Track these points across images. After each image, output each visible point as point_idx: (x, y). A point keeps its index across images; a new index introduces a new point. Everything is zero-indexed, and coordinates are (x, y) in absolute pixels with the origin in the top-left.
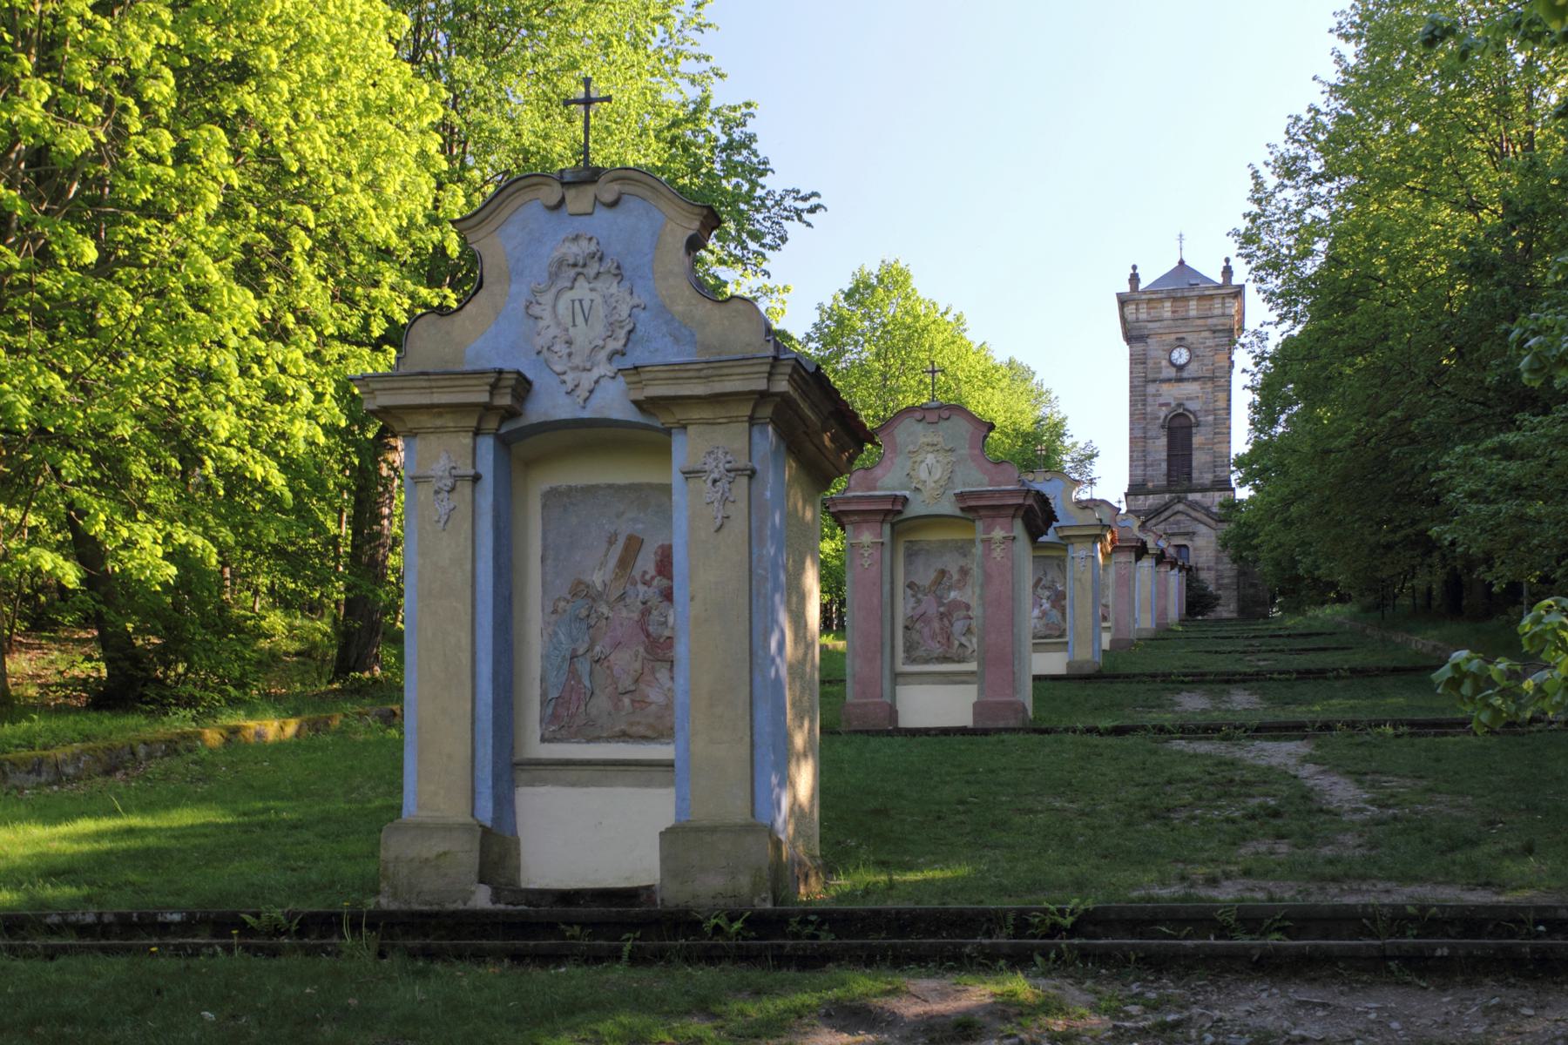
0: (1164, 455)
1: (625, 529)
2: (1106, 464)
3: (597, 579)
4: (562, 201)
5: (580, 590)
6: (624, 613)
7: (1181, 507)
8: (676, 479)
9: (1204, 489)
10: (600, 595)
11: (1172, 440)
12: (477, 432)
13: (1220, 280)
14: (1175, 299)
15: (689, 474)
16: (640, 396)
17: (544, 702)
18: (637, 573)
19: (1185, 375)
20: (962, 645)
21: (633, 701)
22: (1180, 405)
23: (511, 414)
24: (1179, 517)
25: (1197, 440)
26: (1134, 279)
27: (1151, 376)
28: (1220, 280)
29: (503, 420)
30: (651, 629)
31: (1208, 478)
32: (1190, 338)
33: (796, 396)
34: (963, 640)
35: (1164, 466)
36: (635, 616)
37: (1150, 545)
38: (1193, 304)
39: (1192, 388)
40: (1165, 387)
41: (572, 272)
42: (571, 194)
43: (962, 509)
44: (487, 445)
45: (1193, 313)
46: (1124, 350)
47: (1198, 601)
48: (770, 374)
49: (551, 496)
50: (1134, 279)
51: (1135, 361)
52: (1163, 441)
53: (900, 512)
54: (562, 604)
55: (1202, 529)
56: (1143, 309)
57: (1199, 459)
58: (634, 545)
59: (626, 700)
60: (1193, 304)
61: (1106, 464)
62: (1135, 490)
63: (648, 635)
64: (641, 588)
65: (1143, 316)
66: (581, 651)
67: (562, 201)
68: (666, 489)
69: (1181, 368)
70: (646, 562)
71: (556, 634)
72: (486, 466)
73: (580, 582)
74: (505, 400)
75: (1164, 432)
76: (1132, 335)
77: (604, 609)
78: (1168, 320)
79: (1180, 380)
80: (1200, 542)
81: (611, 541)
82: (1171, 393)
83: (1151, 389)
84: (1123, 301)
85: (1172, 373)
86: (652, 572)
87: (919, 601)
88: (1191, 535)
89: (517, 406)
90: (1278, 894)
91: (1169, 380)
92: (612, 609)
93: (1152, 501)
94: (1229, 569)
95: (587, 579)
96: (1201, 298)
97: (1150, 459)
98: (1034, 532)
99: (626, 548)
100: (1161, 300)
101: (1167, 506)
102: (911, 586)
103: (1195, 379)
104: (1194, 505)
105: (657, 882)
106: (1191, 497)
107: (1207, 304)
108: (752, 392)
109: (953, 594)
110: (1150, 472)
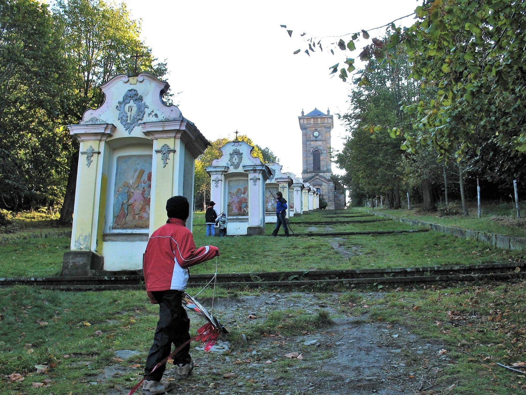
0: (312, 162)
1: (139, 167)
2: (291, 162)
3: (131, 182)
4: (129, 80)
5: (126, 185)
6: (138, 191)
7: (317, 177)
8: (154, 153)
9: (324, 172)
10: (131, 186)
11: (315, 159)
12: (100, 141)
13: (326, 114)
14: (314, 118)
15: (157, 152)
16: (145, 131)
17: (114, 217)
18: (142, 180)
19: (318, 139)
20: (244, 210)
21: (139, 217)
22: (316, 148)
23: (110, 135)
24: (318, 180)
25: (321, 158)
26: (303, 112)
27: (308, 139)
28: (326, 114)
29: (108, 137)
30: (145, 196)
31: (325, 169)
32: (319, 129)
33: (187, 131)
34: (245, 209)
35: (312, 165)
36: (141, 192)
37: (311, 189)
38: (319, 120)
39: (320, 143)
40: (312, 143)
41: (129, 98)
42: (131, 79)
43: (245, 171)
44: (103, 144)
45: (319, 122)
46: (300, 132)
47: (323, 205)
48: (181, 125)
49: (119, 158)
50: (303, 112)
51: (305, 135)
52: (312, 158)
53: (227, 172)
54: (121, 189)
55: (324, 184)
56: (305, 121)
57: (322, 163)
58: (142, 172)
59: (137, 217)
60: (319, 120)
61: (291, 162)
62: (305, 172)
63: (144, 197)
64: (143, 184)
65: (305, 123)
66: (125, 202)
67: (129, 80)
68: (151, 156)
69: (316, 137)
70: (145, 177)
71: (118, 197)
72: (102, 150)
73: (126, 182)
74: (108, 132)
75: (312, 155)
76: (303, 128)
77: (132, 190)
78: (314, 124)
79: (316, 141)
80: (323, 187)
81: (136, 171)
82: (313, 144)
83: (308, 143)
84: (300, 119)
85: (314, 138)
86: (146, 179)
87: (232, 198)
88: (321, 185)
89: (112, 133)
90: (479, 365)
91: (313, 141)
92: (134, 190)
93: (309, 175)
94: (332, 195)
95: (128, 181)
96: (321, 118)
97: (308, 163)
98: (265, 178)
99: (140, 173)
100: (311, 118)
101: (313, 177)
102: (229, 193)
103: (320, 141)
104: (321, 177)
105: (141, 267)
106: (320, 174)
107: (323, 120)
108: (175, 130)
109: (242, 196)
110: (309, 166)
